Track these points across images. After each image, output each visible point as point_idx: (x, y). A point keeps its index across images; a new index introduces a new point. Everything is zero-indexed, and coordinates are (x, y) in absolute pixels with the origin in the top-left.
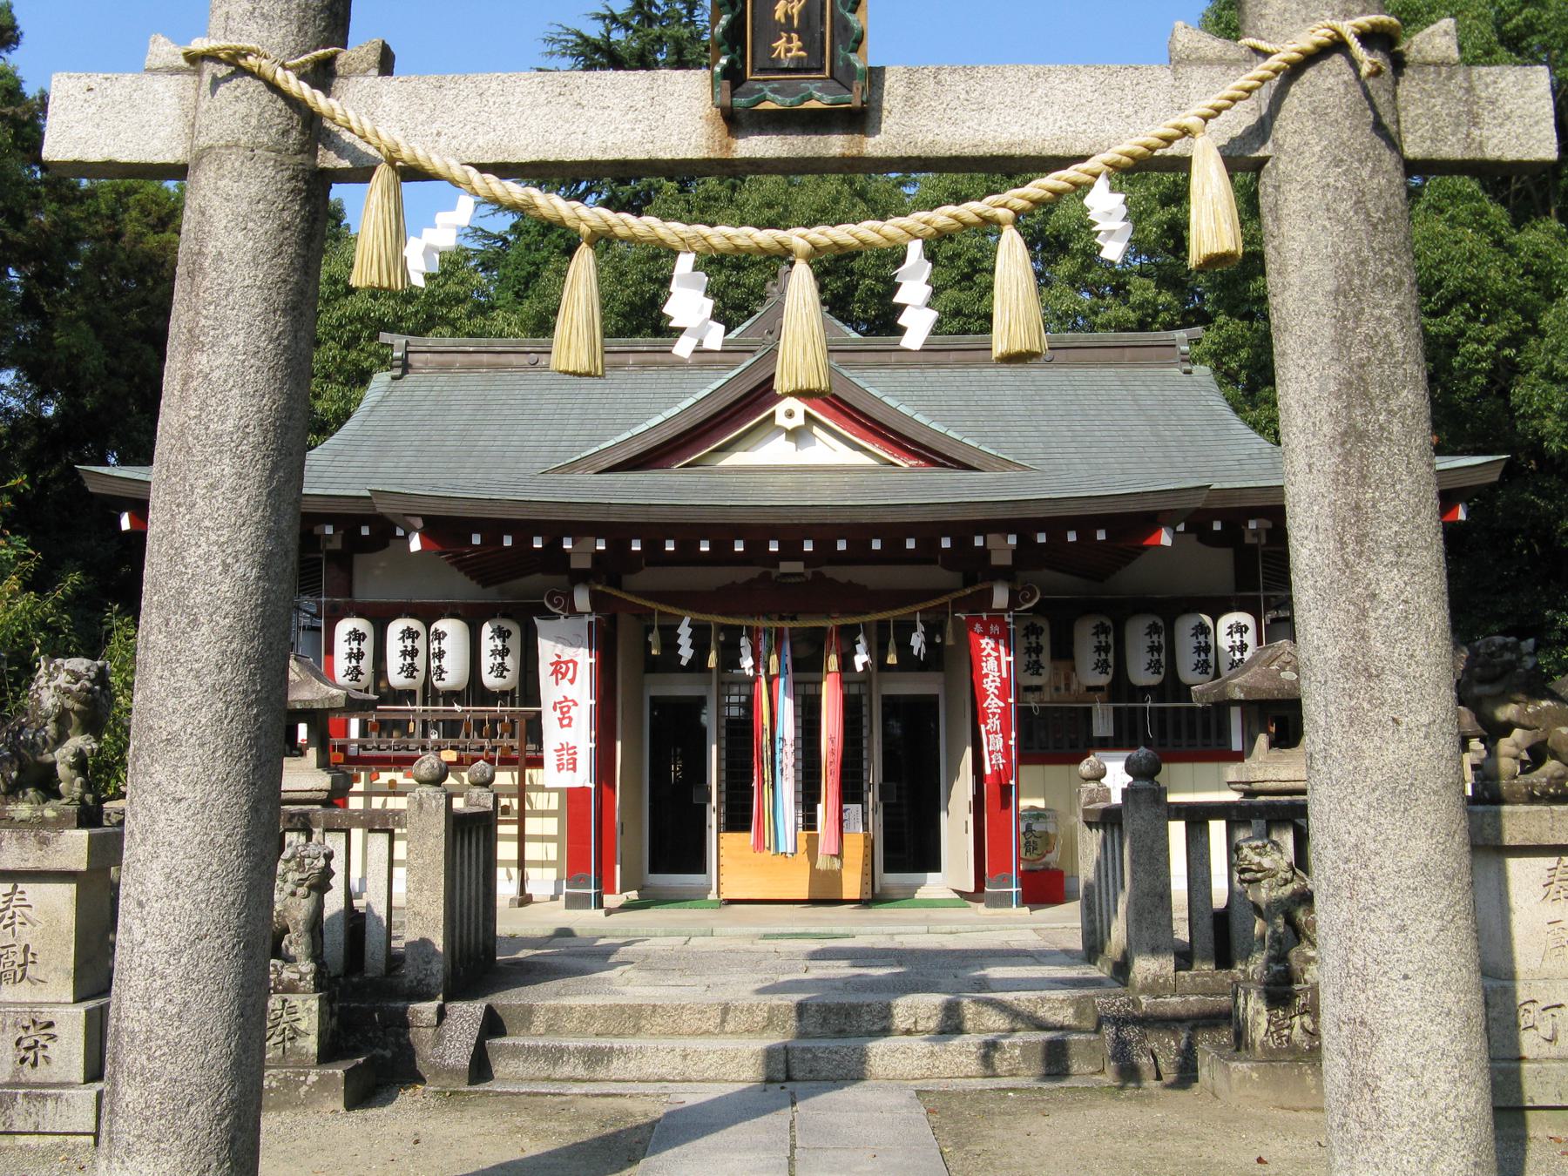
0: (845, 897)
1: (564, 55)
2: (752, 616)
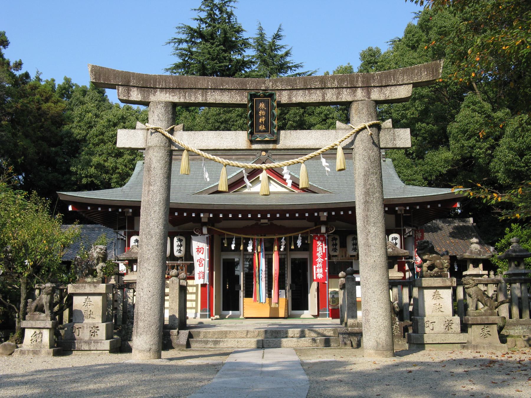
0: (280, 316)
1: (183, 33)
2: (253, 235)
